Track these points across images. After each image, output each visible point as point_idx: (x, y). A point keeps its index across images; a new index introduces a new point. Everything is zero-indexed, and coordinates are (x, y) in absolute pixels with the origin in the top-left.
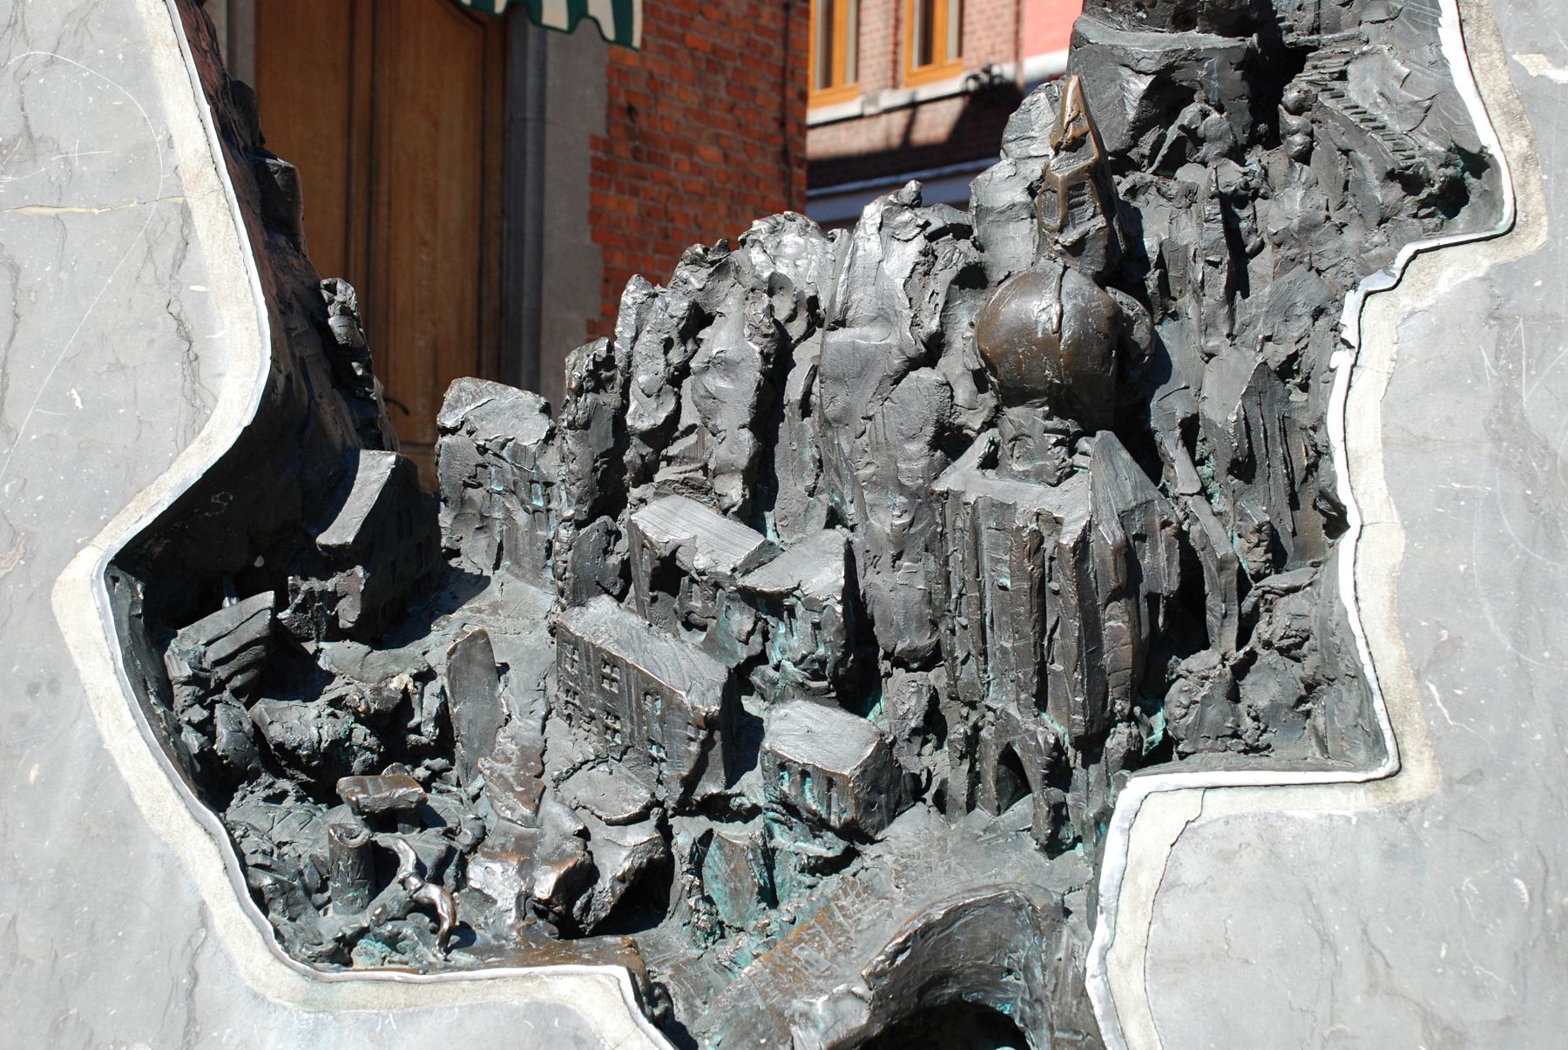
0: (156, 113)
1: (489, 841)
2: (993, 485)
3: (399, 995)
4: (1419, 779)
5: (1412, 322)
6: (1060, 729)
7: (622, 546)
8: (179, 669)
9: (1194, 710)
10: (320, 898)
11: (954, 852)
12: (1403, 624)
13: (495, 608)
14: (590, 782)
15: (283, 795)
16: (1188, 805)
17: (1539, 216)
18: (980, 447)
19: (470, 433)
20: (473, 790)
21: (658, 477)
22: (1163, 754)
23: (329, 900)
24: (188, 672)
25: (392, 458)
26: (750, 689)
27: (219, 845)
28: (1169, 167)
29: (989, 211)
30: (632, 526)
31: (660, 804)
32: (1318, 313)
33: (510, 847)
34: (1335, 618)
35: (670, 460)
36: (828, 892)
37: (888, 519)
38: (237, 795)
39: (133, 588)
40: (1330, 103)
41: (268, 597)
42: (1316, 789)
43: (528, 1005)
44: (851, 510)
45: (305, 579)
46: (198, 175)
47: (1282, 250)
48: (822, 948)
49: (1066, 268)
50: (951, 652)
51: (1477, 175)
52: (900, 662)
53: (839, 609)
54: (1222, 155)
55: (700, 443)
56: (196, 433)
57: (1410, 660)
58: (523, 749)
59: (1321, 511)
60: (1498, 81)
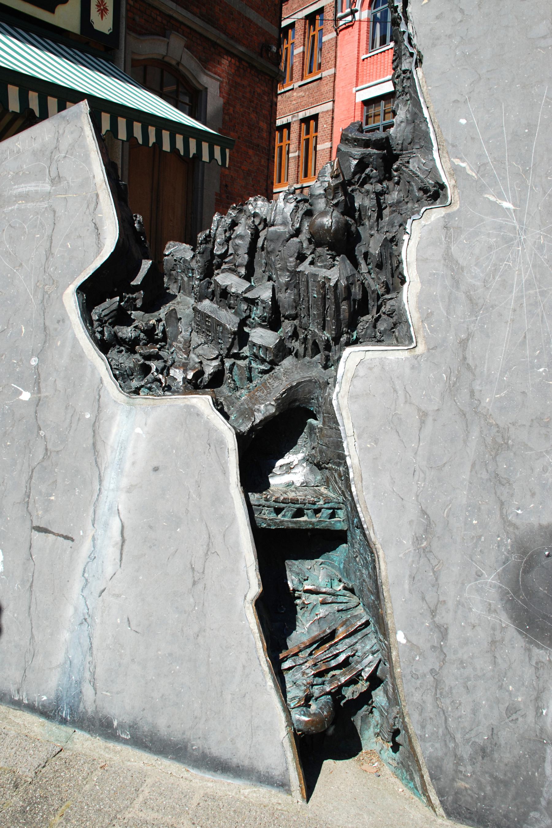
0: (91, 169)
1: (175, 364)
2: (313, 269)
3: (151, 402)
4: (421, 349)
5: (425, 228)
6: (329, 336)
7: (212, 286)
8: (95, 317)
9: (364, 330)
10: (132, 377)
11: (299, 368)
12: (419, 308)
13: (178, 303)
14: (203, 349)
15: (122, 351)
16: (361, 355)
17: (457, 201)
18: (309, 259)
19: (172, 256)
20: (172, 350)
21: (222, 268)
22: (356, 342)
23: (134, 378)
24: (97, 318)
25: (151, 262)
26: (246, 325)
27: (105, 362)
28: (362, 185)
29: (314, 195)
30: (215, 280)
31: (221, 355)
32: (401, 225)
33: (181, 365)
34: (402, 306)
35: (226, 263)
36: (266, 378)
37: (284, 279)
38: (110, 351)
39: (83, 296)
40: (405, 169)
41: (118, 298)
42: (395, 351)
43: (185, 405)
44: (274, 276)
45: (128, 294)
46: (101, 185)
47: (392, 208)
48: (263, 392)
49: (333, 210)
50: (300, 315)
51: (442, 190)
52: (287, 318)
53: (270, 303)
54: (376, 182)
55: (234, 258)
56: (99, 254)
57: (420, 318)
58: (185, 340)
59: (400, 278)
60: (448, 165)
